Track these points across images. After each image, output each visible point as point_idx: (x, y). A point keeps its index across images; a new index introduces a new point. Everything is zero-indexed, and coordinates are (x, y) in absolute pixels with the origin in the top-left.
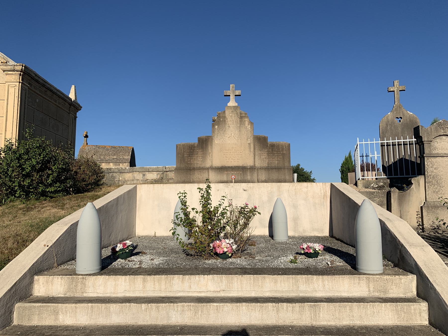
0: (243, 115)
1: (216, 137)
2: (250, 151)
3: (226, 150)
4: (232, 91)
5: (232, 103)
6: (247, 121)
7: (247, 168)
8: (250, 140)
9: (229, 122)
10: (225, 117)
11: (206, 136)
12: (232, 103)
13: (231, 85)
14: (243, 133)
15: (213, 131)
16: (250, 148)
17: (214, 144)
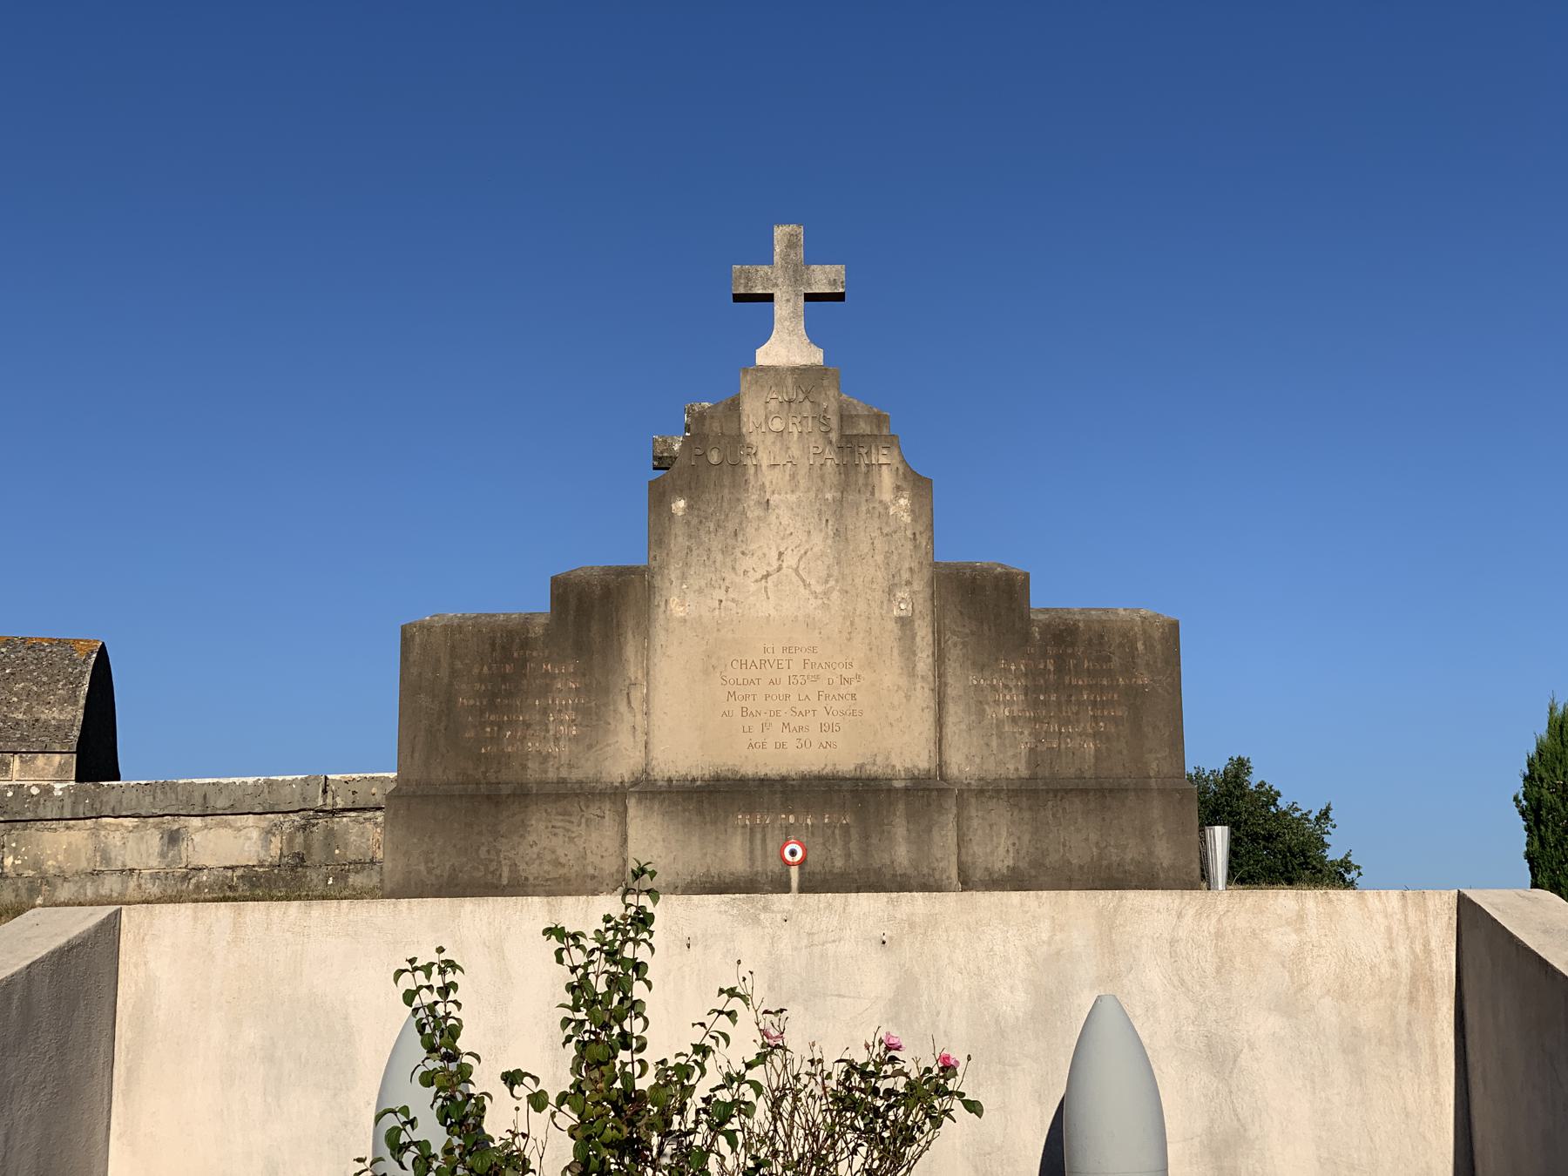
0: (864, 427)
1: (674, 572)
2: (911, 673)
4: (786, 270)
5: (786, 346)
6: (885, 469)
7: (890, 790)
8: (911, 599)
9: (769, 477)
11: (607, 570)
13: (780, 232)
14: (865, 548)
15: (658, 536)
16: (909, 652)
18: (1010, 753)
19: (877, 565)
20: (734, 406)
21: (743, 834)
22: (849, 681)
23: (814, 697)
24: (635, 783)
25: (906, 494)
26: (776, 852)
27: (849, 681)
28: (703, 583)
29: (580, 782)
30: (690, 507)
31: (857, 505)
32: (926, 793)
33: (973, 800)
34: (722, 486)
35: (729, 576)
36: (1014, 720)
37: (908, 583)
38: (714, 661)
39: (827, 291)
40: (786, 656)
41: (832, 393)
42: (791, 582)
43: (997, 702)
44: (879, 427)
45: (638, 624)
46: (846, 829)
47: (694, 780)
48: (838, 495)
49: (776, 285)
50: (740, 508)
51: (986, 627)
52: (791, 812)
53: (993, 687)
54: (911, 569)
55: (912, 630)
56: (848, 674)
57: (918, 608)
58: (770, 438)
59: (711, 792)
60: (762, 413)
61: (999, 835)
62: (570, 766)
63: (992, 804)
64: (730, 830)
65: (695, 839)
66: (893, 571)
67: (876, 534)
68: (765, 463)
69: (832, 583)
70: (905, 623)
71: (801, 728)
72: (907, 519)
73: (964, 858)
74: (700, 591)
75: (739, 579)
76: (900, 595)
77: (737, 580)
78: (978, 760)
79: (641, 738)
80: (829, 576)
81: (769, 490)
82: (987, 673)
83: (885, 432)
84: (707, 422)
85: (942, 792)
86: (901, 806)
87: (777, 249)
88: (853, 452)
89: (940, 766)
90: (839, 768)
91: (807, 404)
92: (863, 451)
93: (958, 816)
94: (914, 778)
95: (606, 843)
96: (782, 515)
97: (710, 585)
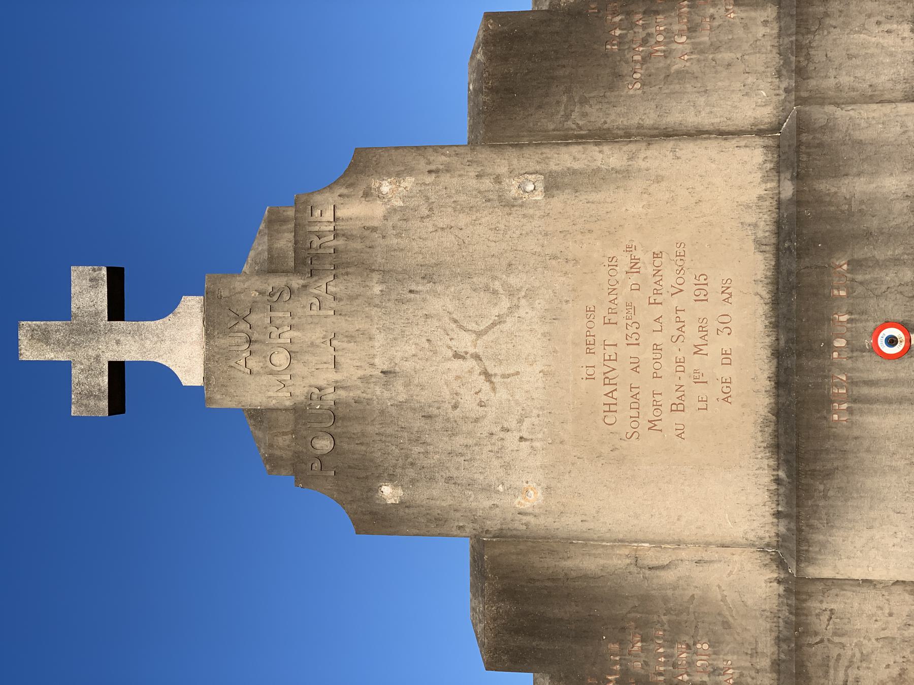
0: (285, 241)
1: (481, 503)
2: (625, 174)
3: (610, 408)
4: (80, 343)
5: (177, 344)
6: (341, 212)
7: (798, 201)
8: (519, 174)
9: (350, 372)
10: (301, 413)
11: (477, 591)
12: (177, 344)
13: (29, 352)
14: (448, 240)
15: (434, 523)
16: (595, 178)
17: (540, 523)
18: (740, 32)
19: (474, 223)
20: (258, 415)
21: (861, 412)
22: (635, 262)
23: (658, 310)
24: (781, 564)
25: (375, 183)
26: (890, 365)
27: (635, 262)
28: (496, 463)
29: (778, 640)
30: (391, 478)
31: (390, 249)
32: (800, 150)
33: (813, 83)
34: (363, 435)
35: (487, 426)
36: (693, 29)
37: (498, 179)
38: (605, 449)
39: (105, 290)
40: (599, 349)
41: (238, 283)
42: (496, 341)
43: (667, 54)
44: (285, 221)
45: (552, 552)
46: (856, 265)
47: (778, 481)
48: (376, 276)
49: (97, 358)
50: (393, 411)
51: (561, 72)
52: (829, 344)
53: (644, 60)
54: (479, 176)
55: (563, 174)
56: (624, 261)
57: (533, 166)
58: (298, 368)
59: (798, 459)
60: (265, 379)
61: (863, 46)
62: (755, 653)
63: (818, 56)
64: (856, 432)
65: (869, 483)
66: (479, 201)
67: (429, 224)
68: (333, 376)
69: (497, 285)
70: (553, 184)
71: (702, 329)
72: (408, 182)
73: (899, 95)
74: (507, 467)
75: (491, 413)
76: (514, 192)
77: (491, 416)
78: (751, 79)
79: (713, 553)
80: (487, 289)
81: (369, 371)
82: (625, 69)
83: (291, 213)
84: (278, 453)
85: (802, 126)
86: (823, 186)
87: (50, 356)
88: (318, 257)
89: (760, 133)
90: (760, 275)
91: (253, 318)
92: (316, 242)
93: (837, 105)
94: (778, 169)
95: (869, 608)
96: (403, 353)
97: (498, 453)
